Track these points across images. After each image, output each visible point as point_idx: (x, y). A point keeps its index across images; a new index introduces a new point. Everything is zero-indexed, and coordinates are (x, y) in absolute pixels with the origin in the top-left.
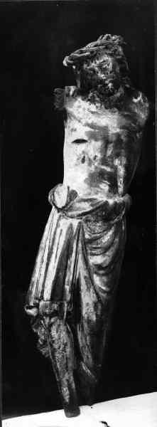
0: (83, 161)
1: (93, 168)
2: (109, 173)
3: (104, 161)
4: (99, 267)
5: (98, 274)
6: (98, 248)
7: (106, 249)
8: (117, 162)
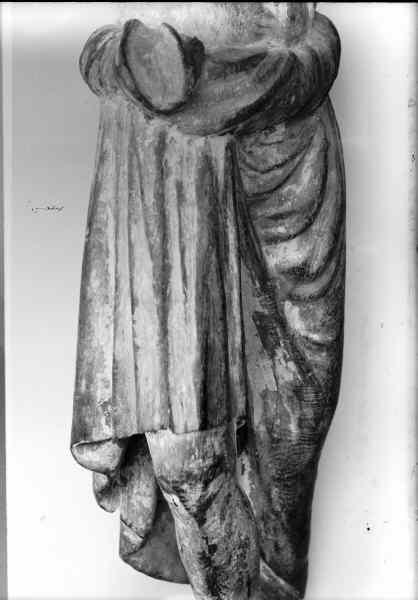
6: (289, 214)
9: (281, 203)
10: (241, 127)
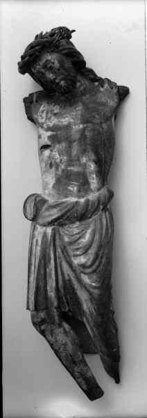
0: (51, 166)
1: (60, 172)
2: (78, 174)
3: (70, 162)
6: (81, 248)
7: (86, 251)
8: (84, 160)
9: (79, 244)
10: (59, 222)
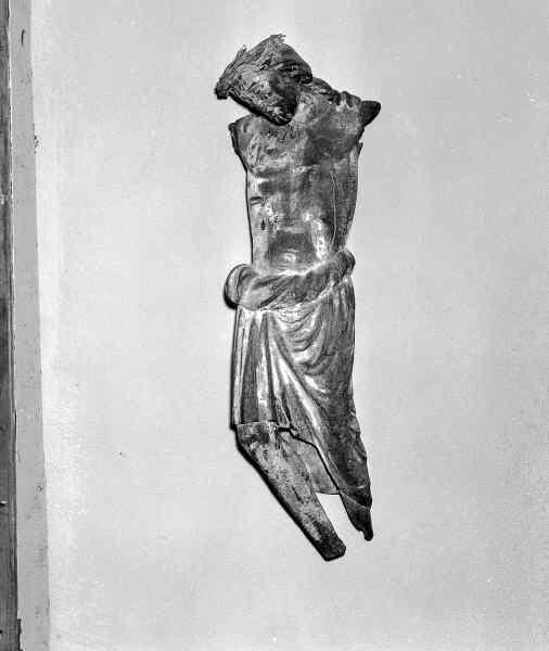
4: (307, 364)
5: (310, 375)
7: (310, 341)
8: (307, 217)
